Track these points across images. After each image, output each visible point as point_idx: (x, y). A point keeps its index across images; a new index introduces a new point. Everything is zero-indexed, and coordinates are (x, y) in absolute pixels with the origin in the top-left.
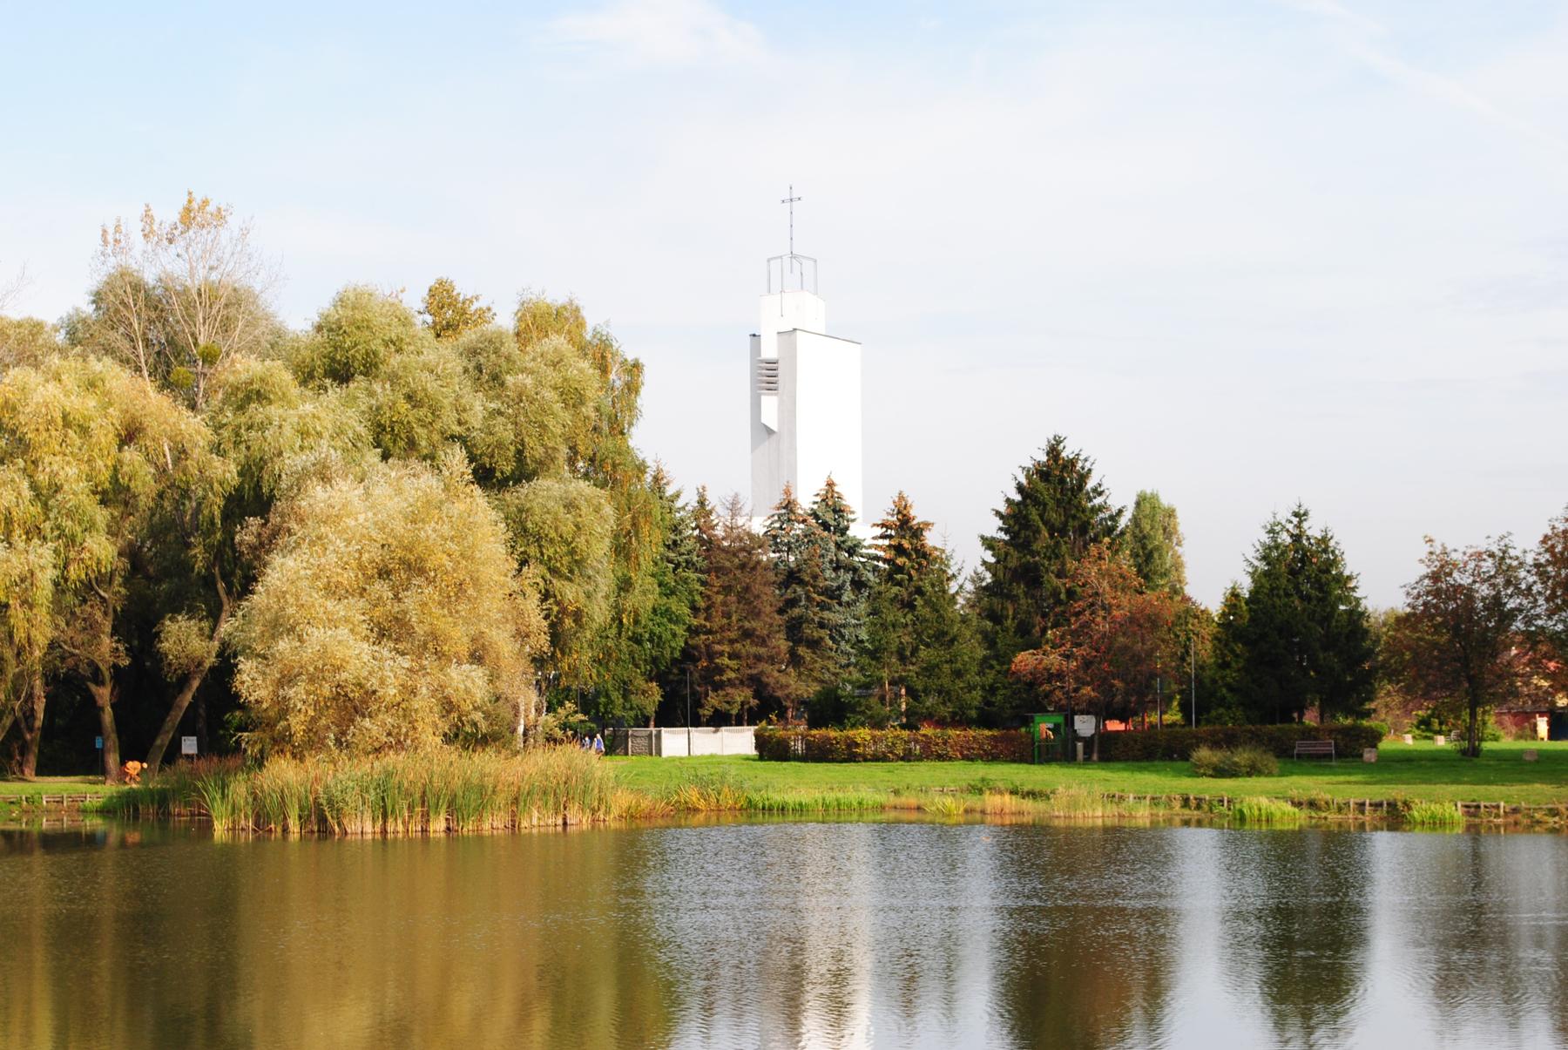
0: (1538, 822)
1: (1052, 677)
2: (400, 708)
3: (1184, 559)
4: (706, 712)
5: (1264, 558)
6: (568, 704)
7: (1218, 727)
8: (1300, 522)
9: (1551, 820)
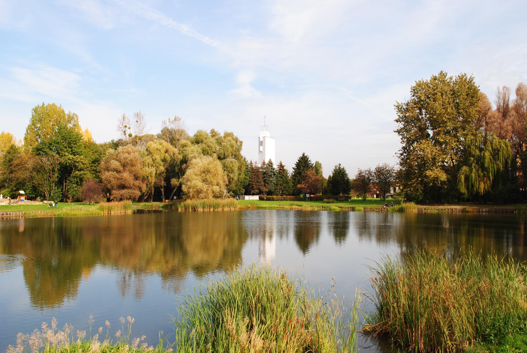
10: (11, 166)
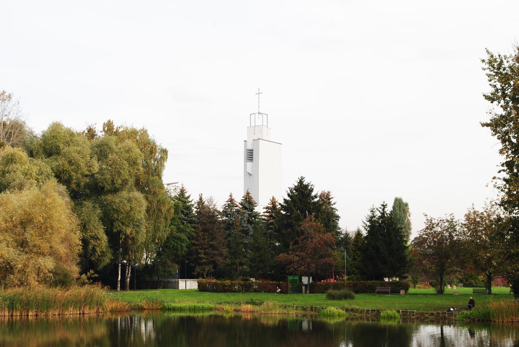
0: (427, 318)
1: (291, 262)
2: (22, 271)
3: (411, 221)
4: (195, 274)
5: (369, 221)
6: (91, 271)
7: (351, 282)
8: (384, 208)
9: (431, 317)
10: (229, 235)
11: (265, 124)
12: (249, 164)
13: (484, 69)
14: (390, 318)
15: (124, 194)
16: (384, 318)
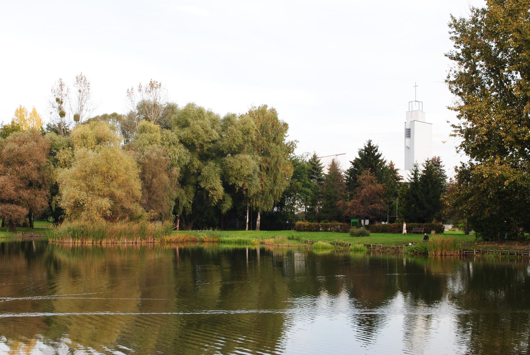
11: (421, 109)
12: (408, 140)
13: (450, 33)
14: (357, 250)
15: (241, 156)
16: (352, 250)
